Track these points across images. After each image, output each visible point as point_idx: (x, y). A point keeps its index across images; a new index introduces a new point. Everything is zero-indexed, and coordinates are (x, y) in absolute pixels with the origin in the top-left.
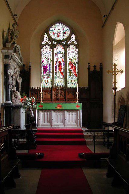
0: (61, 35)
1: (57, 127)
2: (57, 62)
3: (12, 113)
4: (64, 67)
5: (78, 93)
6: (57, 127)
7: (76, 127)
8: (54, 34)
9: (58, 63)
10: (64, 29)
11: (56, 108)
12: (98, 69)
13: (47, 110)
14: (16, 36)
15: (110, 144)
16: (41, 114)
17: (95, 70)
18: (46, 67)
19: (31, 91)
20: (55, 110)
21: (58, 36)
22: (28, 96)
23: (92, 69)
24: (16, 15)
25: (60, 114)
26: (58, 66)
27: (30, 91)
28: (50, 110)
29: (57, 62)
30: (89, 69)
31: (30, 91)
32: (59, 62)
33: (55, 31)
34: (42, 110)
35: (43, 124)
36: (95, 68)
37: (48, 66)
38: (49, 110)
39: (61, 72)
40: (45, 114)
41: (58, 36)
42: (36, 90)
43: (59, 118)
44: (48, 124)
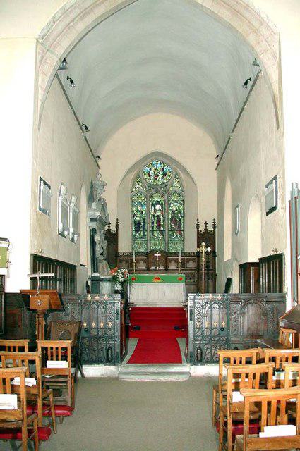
0: (160, 178)
2: (154, 216)
3: (137, 306)
4: (223, 354)
8: (150, 175)
9: (156, 219)
10: (163, 169)
12: (210, 228)
15: (269, 222)
17: (206, 230)
18: (139, 223)
21: (156, 179)
22: (119, 269)
23: (202, 228)
24: (99, 157)
26: (155, 223)
29: (154, 216)
30: (198, 228)
32: (158, 216)
33: (151, 172)
36: (206, 227)
37: (142, 221)
39: (160, 230)
41: (156, 179)
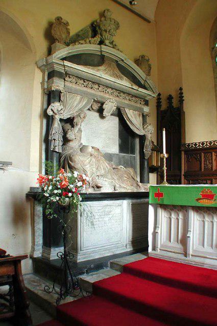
1: (202, 260)
5: (166, 156)
6: (202, 260)
7: (182, 257)
11: (198, 200)
13: (203, 207)
14: (106, 31)
16: (163, 215)
19: (185, 154)
20: (197, 209)
25: (204, 221)
27: (183, 153)
28: (185, 206)
31: (183, 153)
34: (164, 207)
35: (166, 246)
38: (183, 208)
40: (173, 216)
42: (196, 150)
43: (176, 226)
44: (179, 246)
